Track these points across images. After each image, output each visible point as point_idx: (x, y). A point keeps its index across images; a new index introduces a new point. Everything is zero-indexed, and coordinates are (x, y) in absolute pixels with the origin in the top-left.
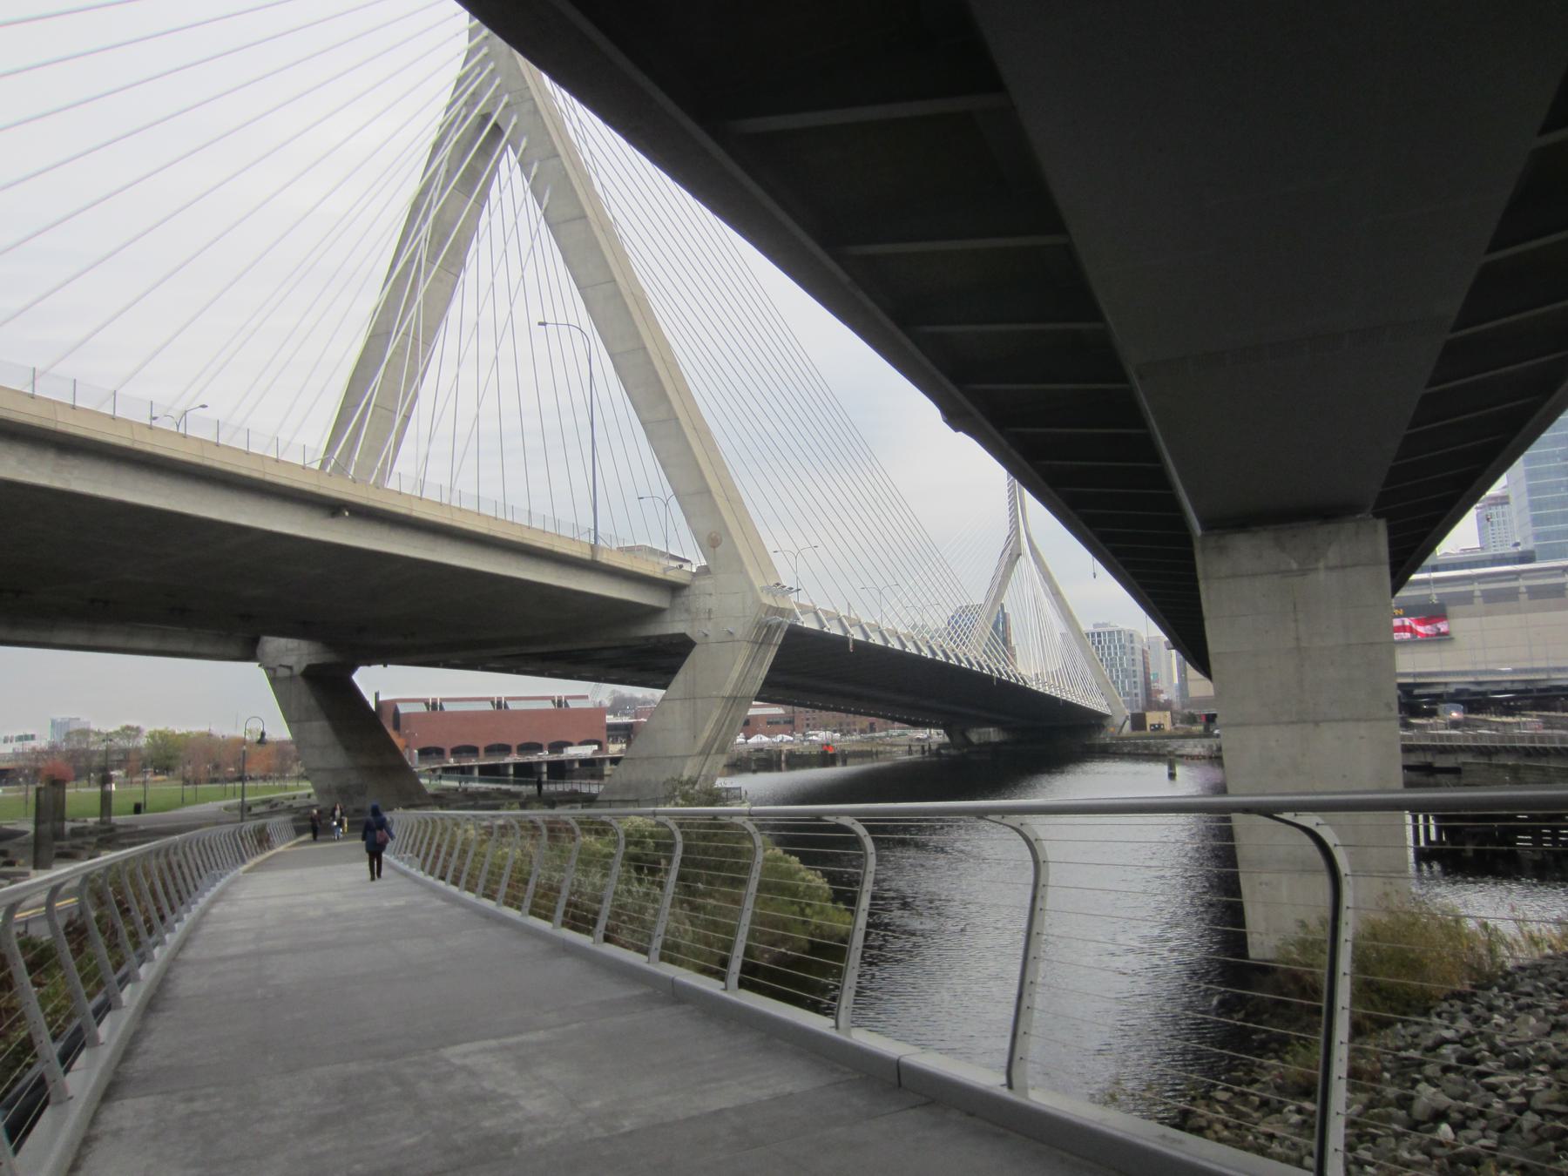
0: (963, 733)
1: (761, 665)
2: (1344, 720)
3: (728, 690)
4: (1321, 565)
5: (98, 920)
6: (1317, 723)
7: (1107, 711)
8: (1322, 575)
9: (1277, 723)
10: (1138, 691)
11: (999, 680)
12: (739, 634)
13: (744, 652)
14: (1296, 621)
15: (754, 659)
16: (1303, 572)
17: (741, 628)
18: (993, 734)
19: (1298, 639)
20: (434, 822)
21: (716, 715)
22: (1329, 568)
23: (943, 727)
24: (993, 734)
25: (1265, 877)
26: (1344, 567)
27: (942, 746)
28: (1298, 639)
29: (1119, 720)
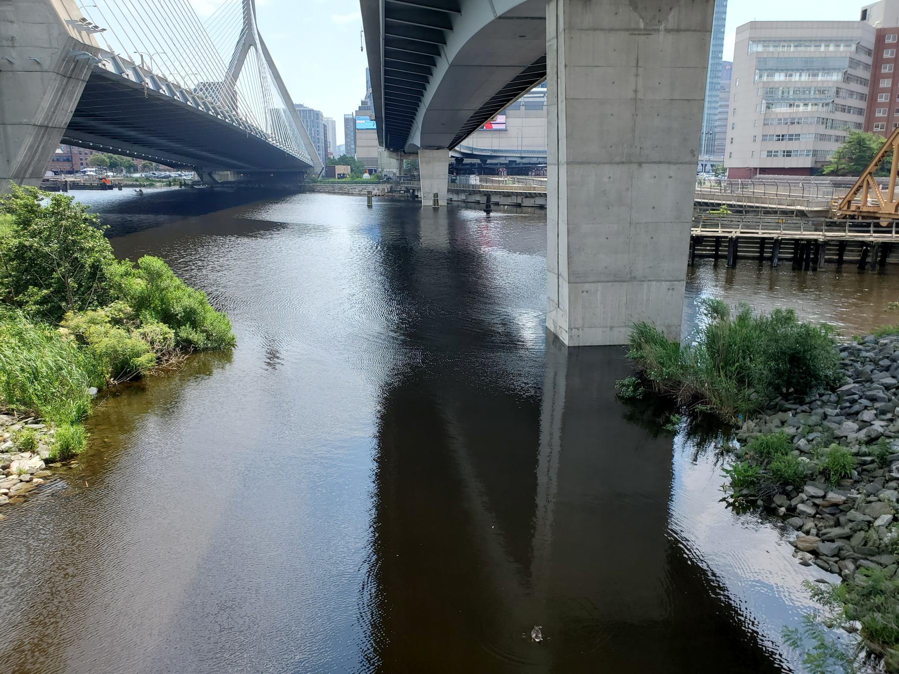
0: (210, 175)
1: (71, 99)
2: (660, 162)
3: (39, 119)
4: (662, 27)
5: (56, 173)
6: (640, 164)
7: (311, 163)
8: (661, 36)
9: (610, 163)
10: (321, 152)
11: (250, 134)
12: (46, 65)
13: (54, 83)
14: (637, 75)
15: (63, 91)
16: (648, 32)
17: (48, 60)
18: (229, 176)
19: (636, 91)
20: (765, 66)
21: (29, 140)
22: (668, 31)
23: (195, 169)
24: (229, 176)
25: (587, 286)
26: (678, 31)
27: (195, 183)
28: (636, 91)
29: (318, 170)
